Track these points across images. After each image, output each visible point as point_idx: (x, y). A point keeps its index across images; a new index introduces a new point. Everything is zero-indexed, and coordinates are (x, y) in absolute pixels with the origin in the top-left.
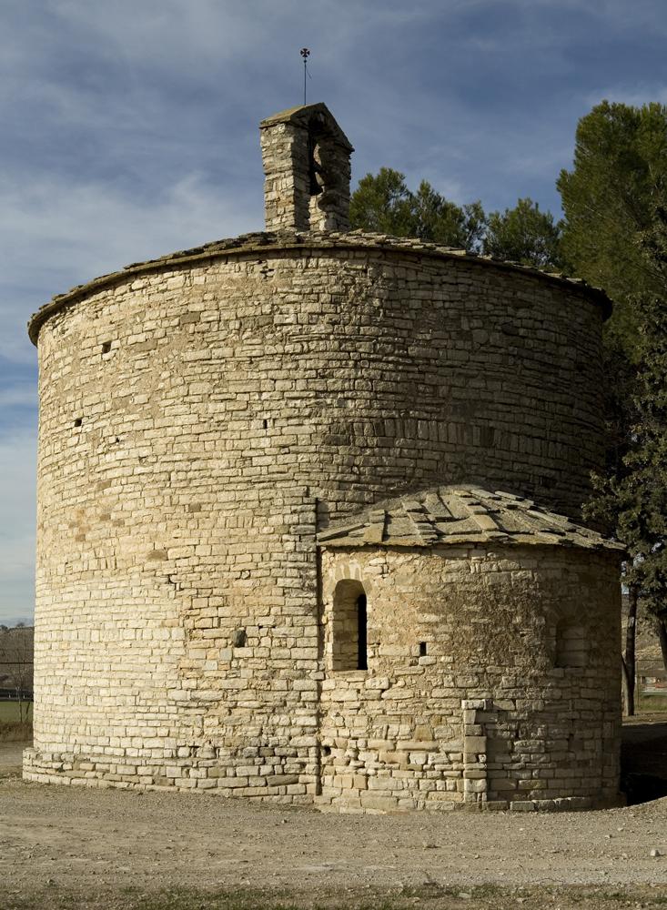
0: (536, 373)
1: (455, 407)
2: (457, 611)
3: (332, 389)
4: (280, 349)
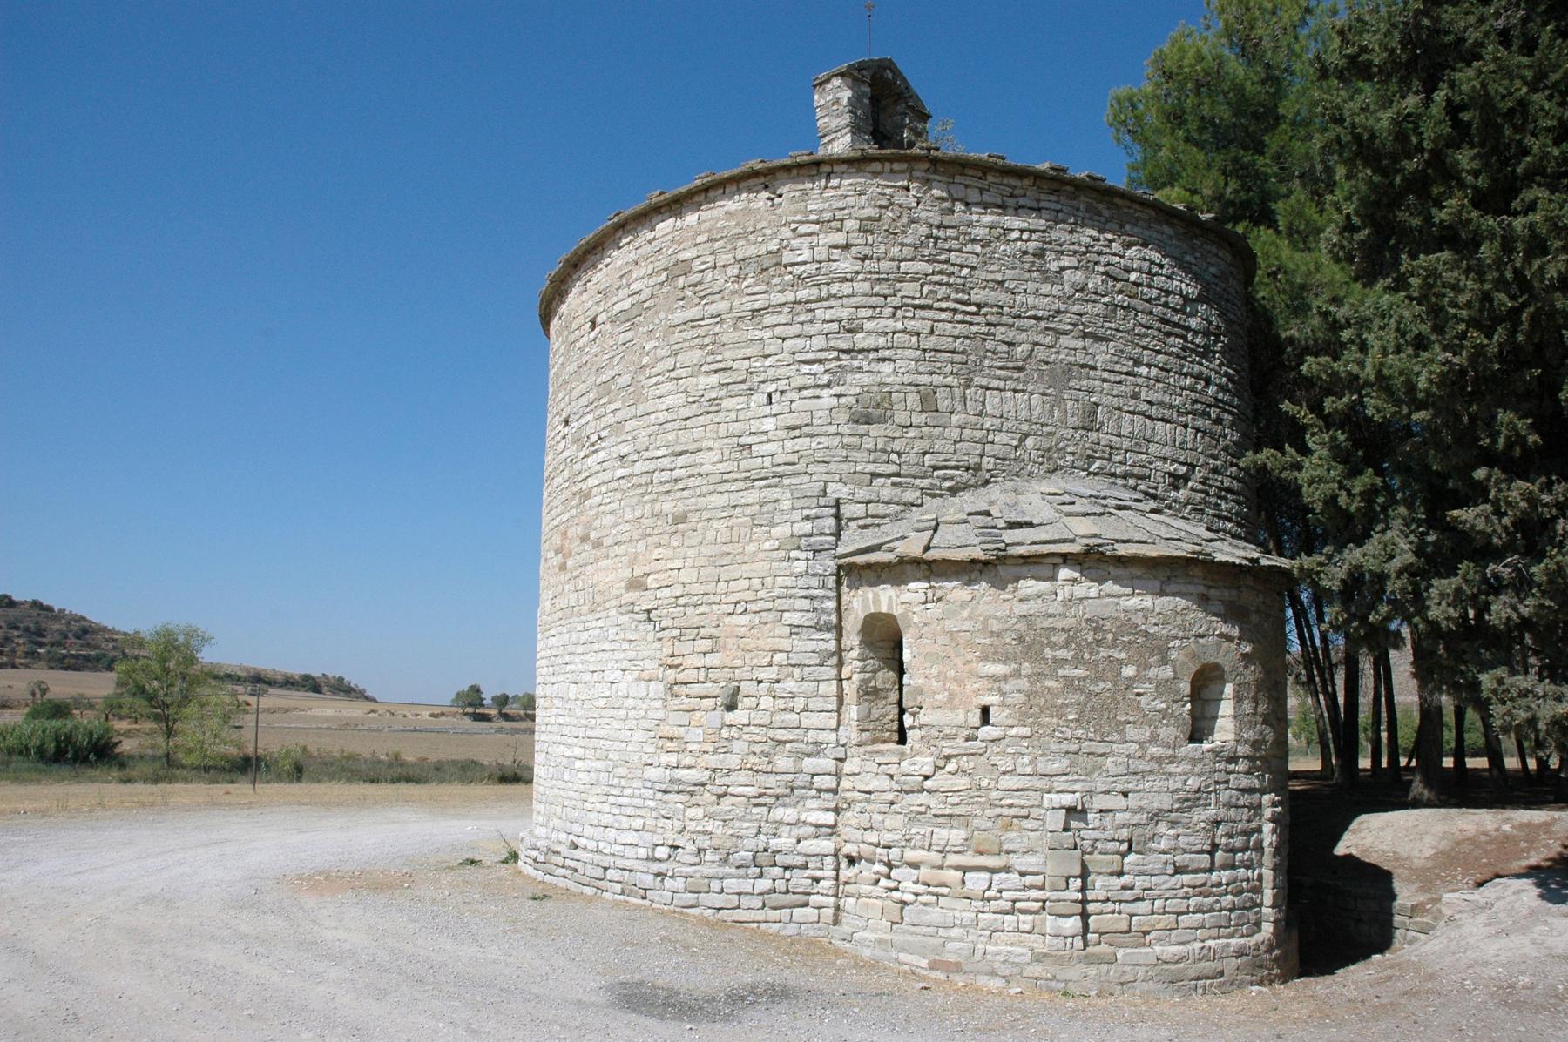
2: (1039, 657)
3: (861, 347)
4: (790, 296)
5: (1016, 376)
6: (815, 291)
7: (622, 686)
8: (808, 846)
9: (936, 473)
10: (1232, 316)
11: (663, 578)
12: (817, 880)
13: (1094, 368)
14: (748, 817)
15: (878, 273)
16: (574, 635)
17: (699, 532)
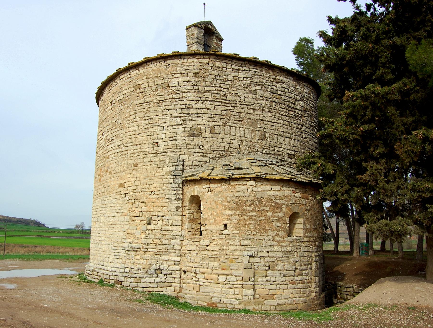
0: (286, 110)
1: (248, 122)
2: (241, 209)
4: (171, 97)
5: (240, 123)
6: (178, 95)
7: (117, 217)
8: (172, 268)
9: (214, 152)
10: (312, 105)
11: (130, 184)
12: (174, 278)
13: (265, 121)
14: (154, 258)
15: (198, 90)
16: (103, 202)
17: (141, 169)
